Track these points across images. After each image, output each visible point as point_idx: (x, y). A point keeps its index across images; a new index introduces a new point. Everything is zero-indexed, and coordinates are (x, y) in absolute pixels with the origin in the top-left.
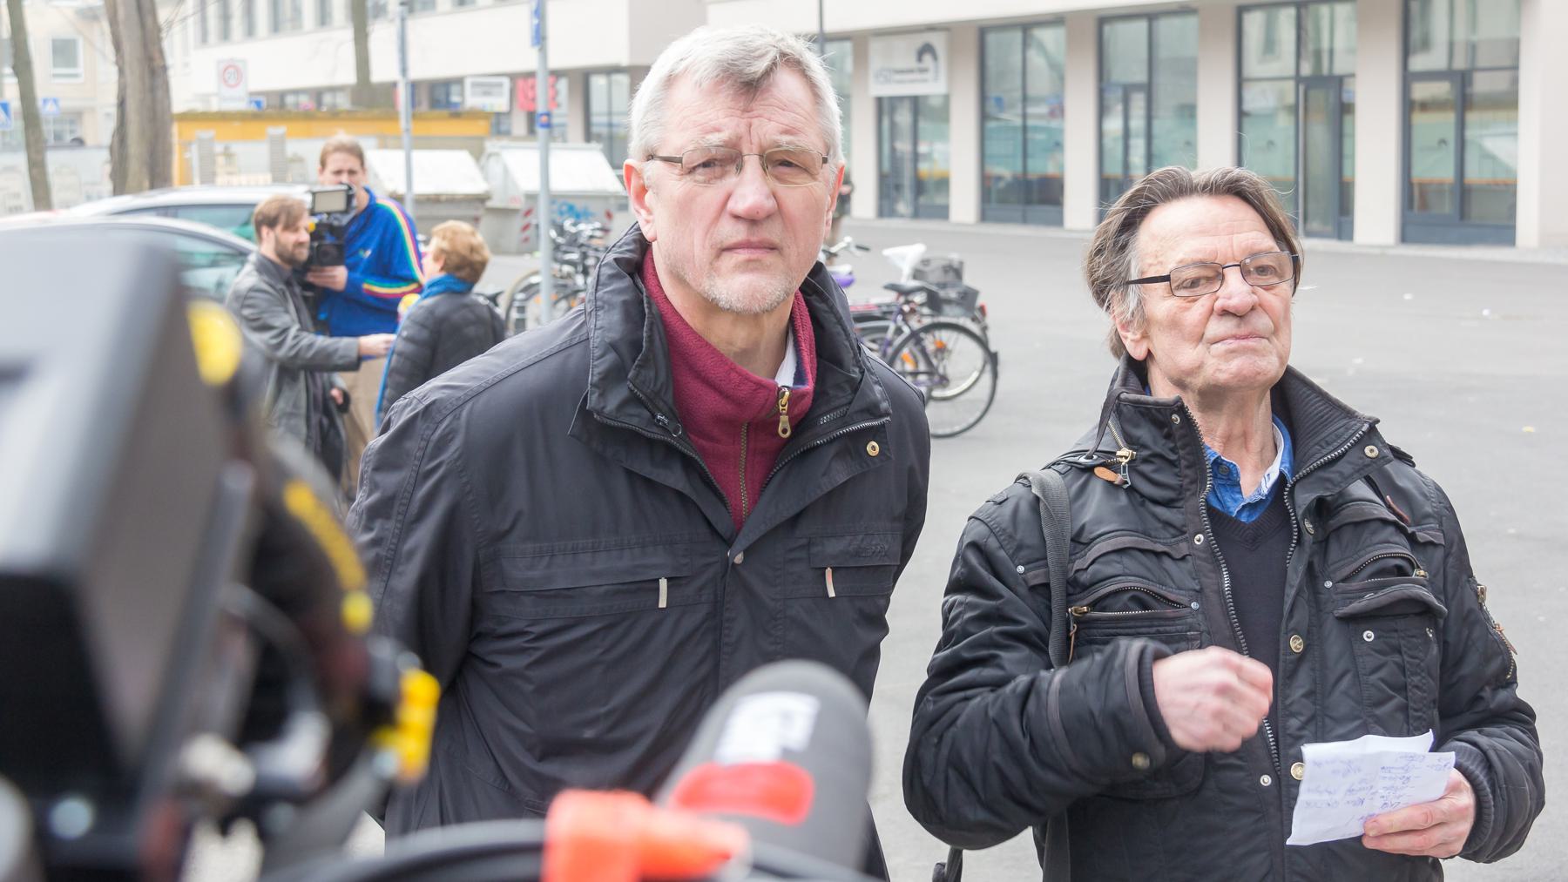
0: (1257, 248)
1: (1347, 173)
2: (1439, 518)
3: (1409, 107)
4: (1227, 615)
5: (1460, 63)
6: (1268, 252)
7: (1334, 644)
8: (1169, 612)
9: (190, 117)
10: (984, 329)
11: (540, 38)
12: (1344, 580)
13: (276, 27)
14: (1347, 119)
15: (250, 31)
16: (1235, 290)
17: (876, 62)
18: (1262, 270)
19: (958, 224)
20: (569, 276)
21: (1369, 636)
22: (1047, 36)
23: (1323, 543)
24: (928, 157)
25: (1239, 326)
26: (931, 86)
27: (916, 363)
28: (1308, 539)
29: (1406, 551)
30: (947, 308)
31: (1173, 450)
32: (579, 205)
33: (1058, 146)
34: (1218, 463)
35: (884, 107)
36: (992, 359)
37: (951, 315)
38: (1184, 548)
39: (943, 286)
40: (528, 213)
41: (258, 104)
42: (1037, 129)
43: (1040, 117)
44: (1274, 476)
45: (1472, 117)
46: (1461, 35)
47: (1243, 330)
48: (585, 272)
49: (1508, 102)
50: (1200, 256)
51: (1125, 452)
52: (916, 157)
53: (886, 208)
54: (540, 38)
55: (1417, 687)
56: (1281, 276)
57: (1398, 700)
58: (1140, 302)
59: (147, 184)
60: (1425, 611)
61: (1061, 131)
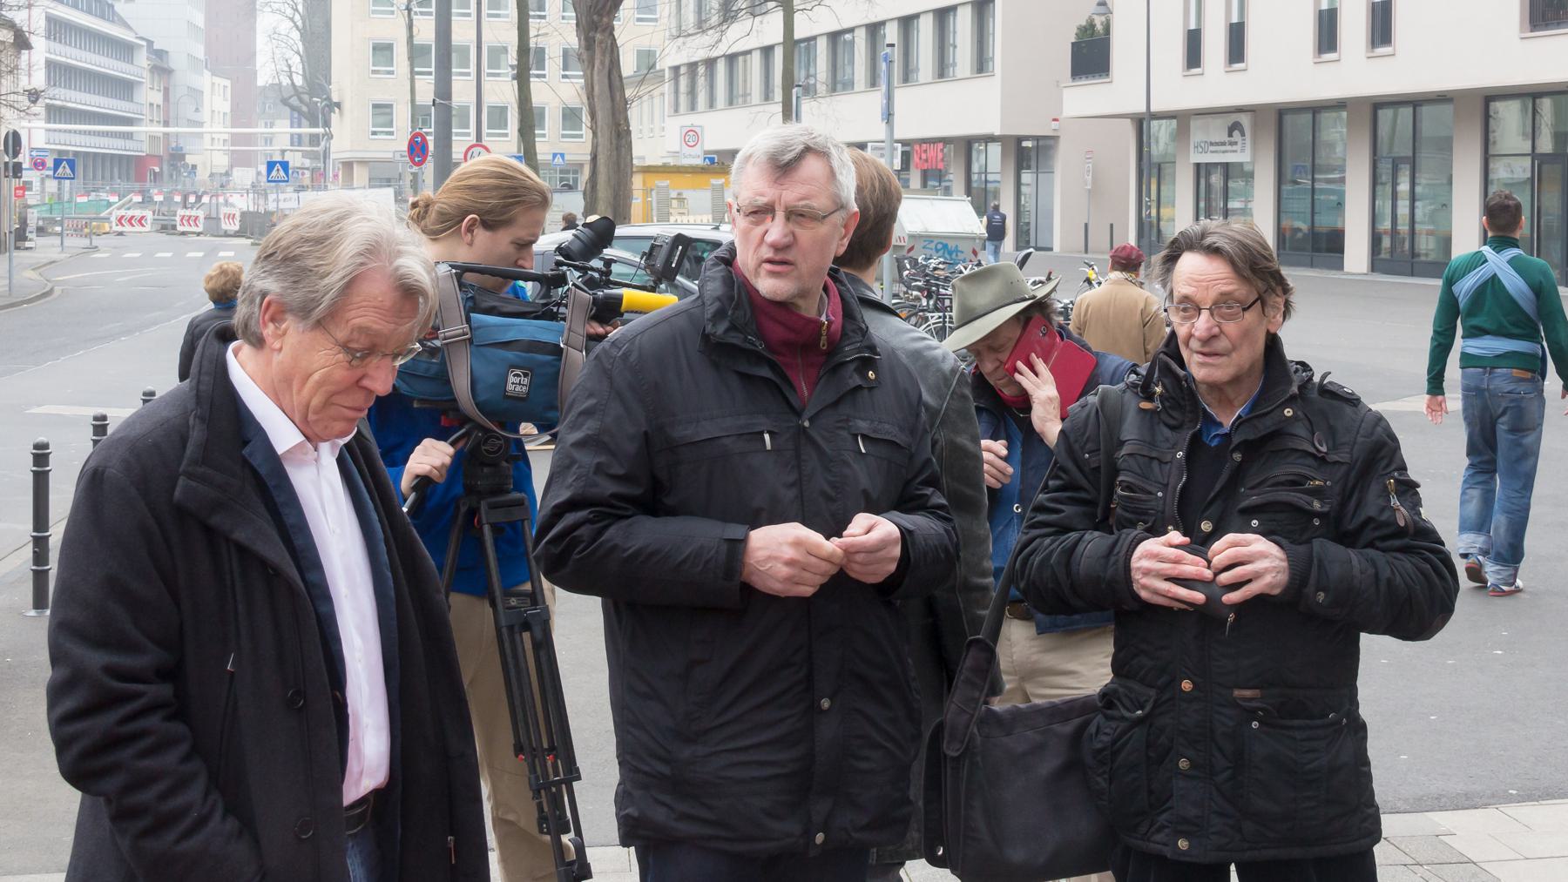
8: (1143, 497)
9: (648, 170)
11: (889, 116)
13: (731, 102)
15: (711, 104)
32: (952, 244)
33: (1340, 205)
40: (911, 249)
41: (712, 160)
42: (1323, 191)
43: (1329, 181)
48: (929, 297)
54: (889, 116)
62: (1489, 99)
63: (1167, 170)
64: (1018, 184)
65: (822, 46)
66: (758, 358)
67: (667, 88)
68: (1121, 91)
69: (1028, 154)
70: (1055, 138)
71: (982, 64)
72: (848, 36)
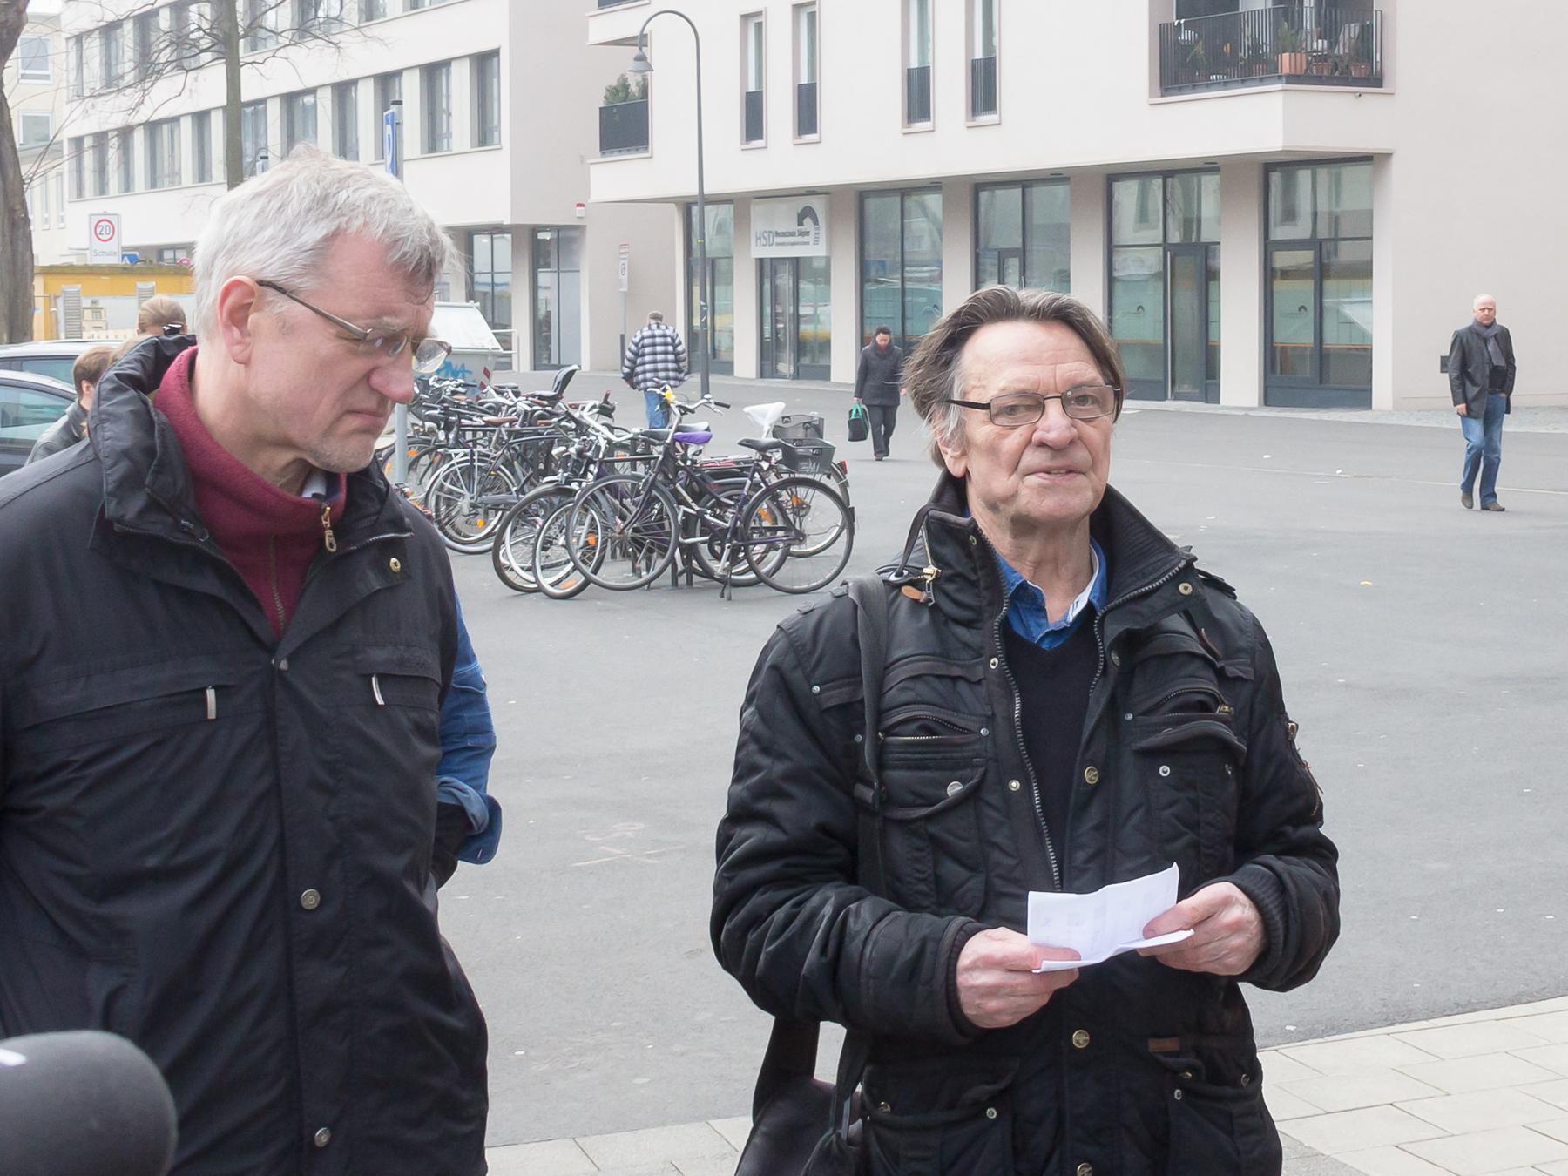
0: (1080, 379)
1: (1212, 338)
2: (1251, 652)
3: (1270, 274)
4: (1013, 737)
5: (1323, 233)
6: (1090, 384)
7: (1129, 767)
8: (957, 738)
9: (50, 271)
10: (844, 486)
12: (1144, 713)
14: (1212, 284)
15: (127, 186)
16: (1054, 423)
17: (757, 225)
18: (1082, 400)
19: (840, 385)
20: (431, 432)
21: (1165, 771)
22: (934, 201)
23: (1127, 676)
24: (814, 319)
25: (1053, 457)
26: (812, 248)
27: (775, 520)
28: (1113, 672)
29: (1213, 688)
30: (803, 465)
31: (974, 570)
34: (1023, 586)
35: (766, 269)
36: (849, 514)
37: (808, 471)
38: (979, 673)
39: (800, 442)
43: (921, 280)
44: (1082, 604)
45: (1329, 285)
46: (1323, 206)
47: (1059, 462)
48: (448, 429)
49: (1363, 271)
50: (1023, 386)
51: (930, 570)
52: (797, 318)
53: (767, 367)
55: (1209, 824)
56: (1104, 411)
57: (1189, 837)
58: (961, 424)
59: (5, 337)
60: (1224, 747)
61: (940, 294)
62: (1112, 177)
63: (722, 265)
64: (534, 288)
65: (274, 110)
66: (199, 560)
67: (67, 166)
68: (664, 169)
69: (545, 247)
70: (580, 228)
71: (484, 135)
72: (308, 99)
